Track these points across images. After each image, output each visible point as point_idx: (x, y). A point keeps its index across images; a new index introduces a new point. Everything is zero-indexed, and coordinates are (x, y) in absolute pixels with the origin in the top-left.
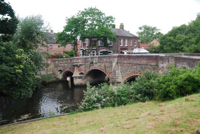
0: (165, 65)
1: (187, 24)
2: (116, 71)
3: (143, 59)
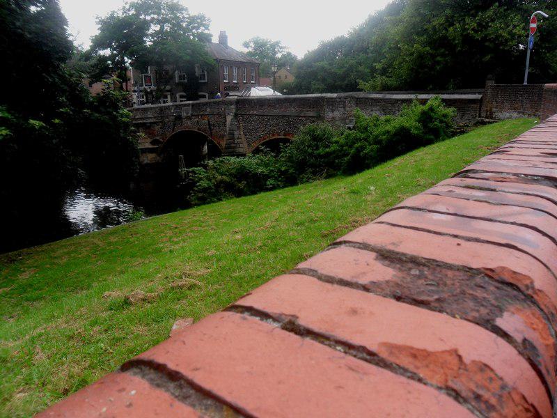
0: (337, 114)
1: (346, 36)
2: (235, 133)
3: (291, 105)
